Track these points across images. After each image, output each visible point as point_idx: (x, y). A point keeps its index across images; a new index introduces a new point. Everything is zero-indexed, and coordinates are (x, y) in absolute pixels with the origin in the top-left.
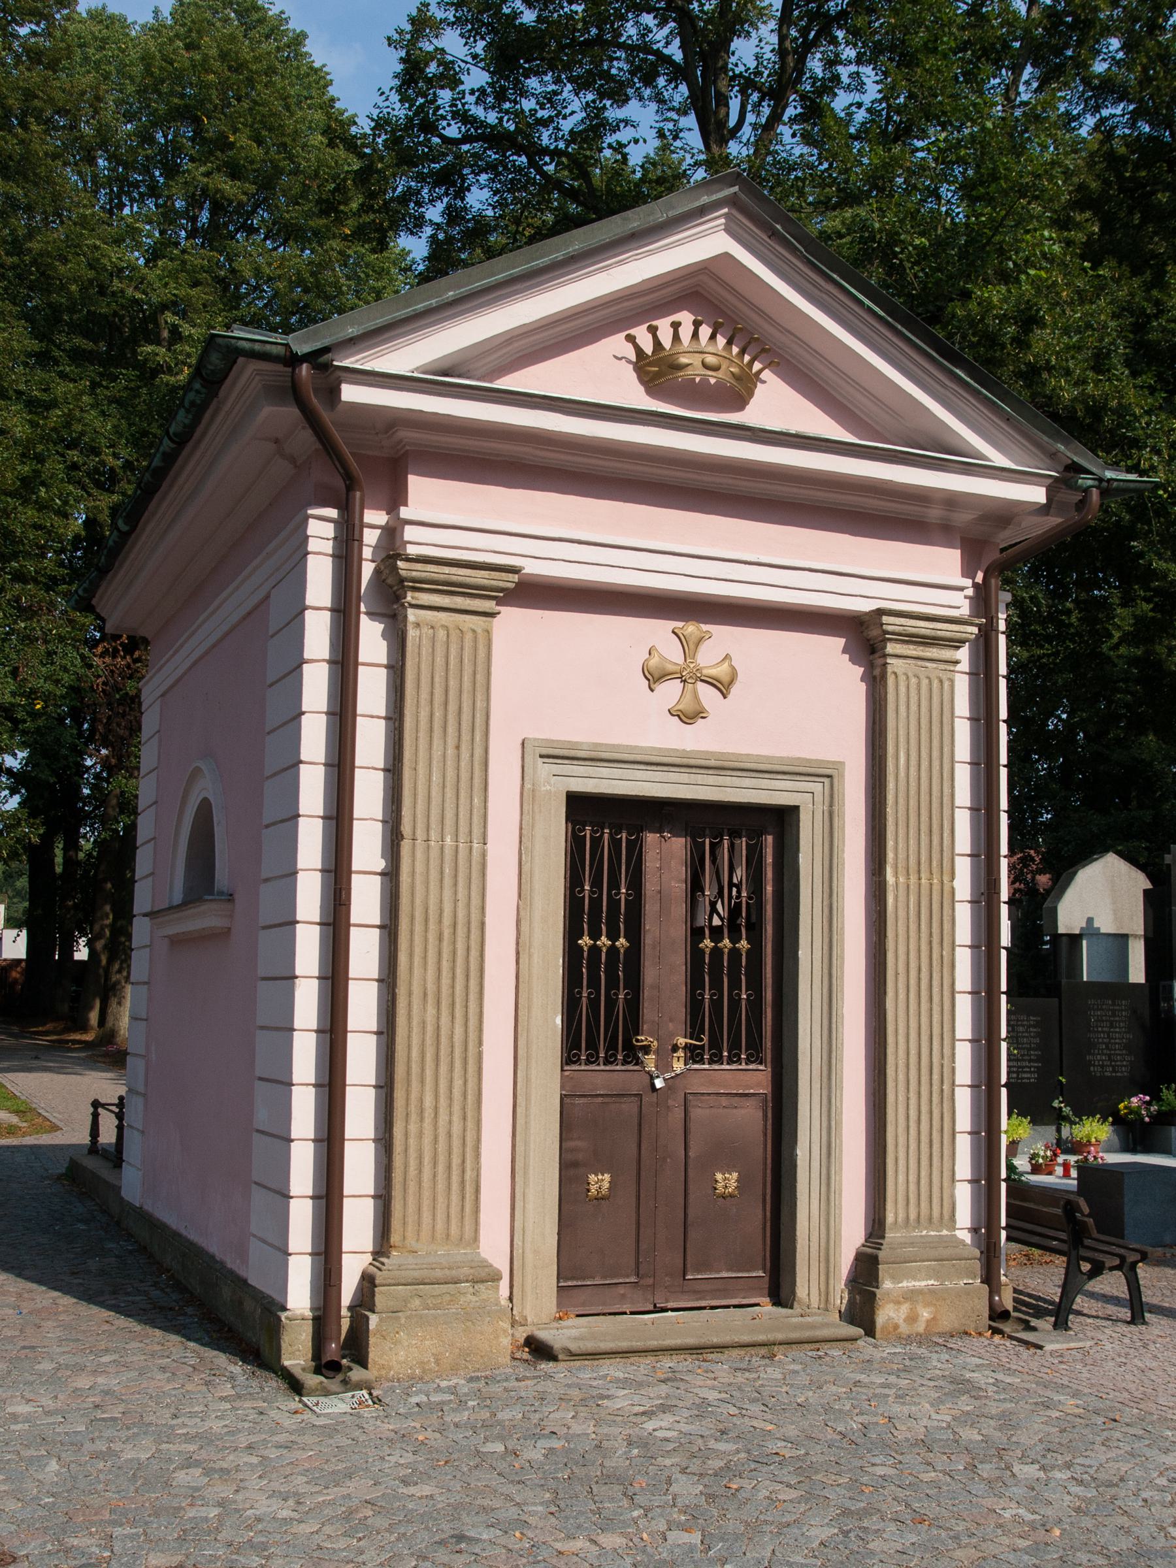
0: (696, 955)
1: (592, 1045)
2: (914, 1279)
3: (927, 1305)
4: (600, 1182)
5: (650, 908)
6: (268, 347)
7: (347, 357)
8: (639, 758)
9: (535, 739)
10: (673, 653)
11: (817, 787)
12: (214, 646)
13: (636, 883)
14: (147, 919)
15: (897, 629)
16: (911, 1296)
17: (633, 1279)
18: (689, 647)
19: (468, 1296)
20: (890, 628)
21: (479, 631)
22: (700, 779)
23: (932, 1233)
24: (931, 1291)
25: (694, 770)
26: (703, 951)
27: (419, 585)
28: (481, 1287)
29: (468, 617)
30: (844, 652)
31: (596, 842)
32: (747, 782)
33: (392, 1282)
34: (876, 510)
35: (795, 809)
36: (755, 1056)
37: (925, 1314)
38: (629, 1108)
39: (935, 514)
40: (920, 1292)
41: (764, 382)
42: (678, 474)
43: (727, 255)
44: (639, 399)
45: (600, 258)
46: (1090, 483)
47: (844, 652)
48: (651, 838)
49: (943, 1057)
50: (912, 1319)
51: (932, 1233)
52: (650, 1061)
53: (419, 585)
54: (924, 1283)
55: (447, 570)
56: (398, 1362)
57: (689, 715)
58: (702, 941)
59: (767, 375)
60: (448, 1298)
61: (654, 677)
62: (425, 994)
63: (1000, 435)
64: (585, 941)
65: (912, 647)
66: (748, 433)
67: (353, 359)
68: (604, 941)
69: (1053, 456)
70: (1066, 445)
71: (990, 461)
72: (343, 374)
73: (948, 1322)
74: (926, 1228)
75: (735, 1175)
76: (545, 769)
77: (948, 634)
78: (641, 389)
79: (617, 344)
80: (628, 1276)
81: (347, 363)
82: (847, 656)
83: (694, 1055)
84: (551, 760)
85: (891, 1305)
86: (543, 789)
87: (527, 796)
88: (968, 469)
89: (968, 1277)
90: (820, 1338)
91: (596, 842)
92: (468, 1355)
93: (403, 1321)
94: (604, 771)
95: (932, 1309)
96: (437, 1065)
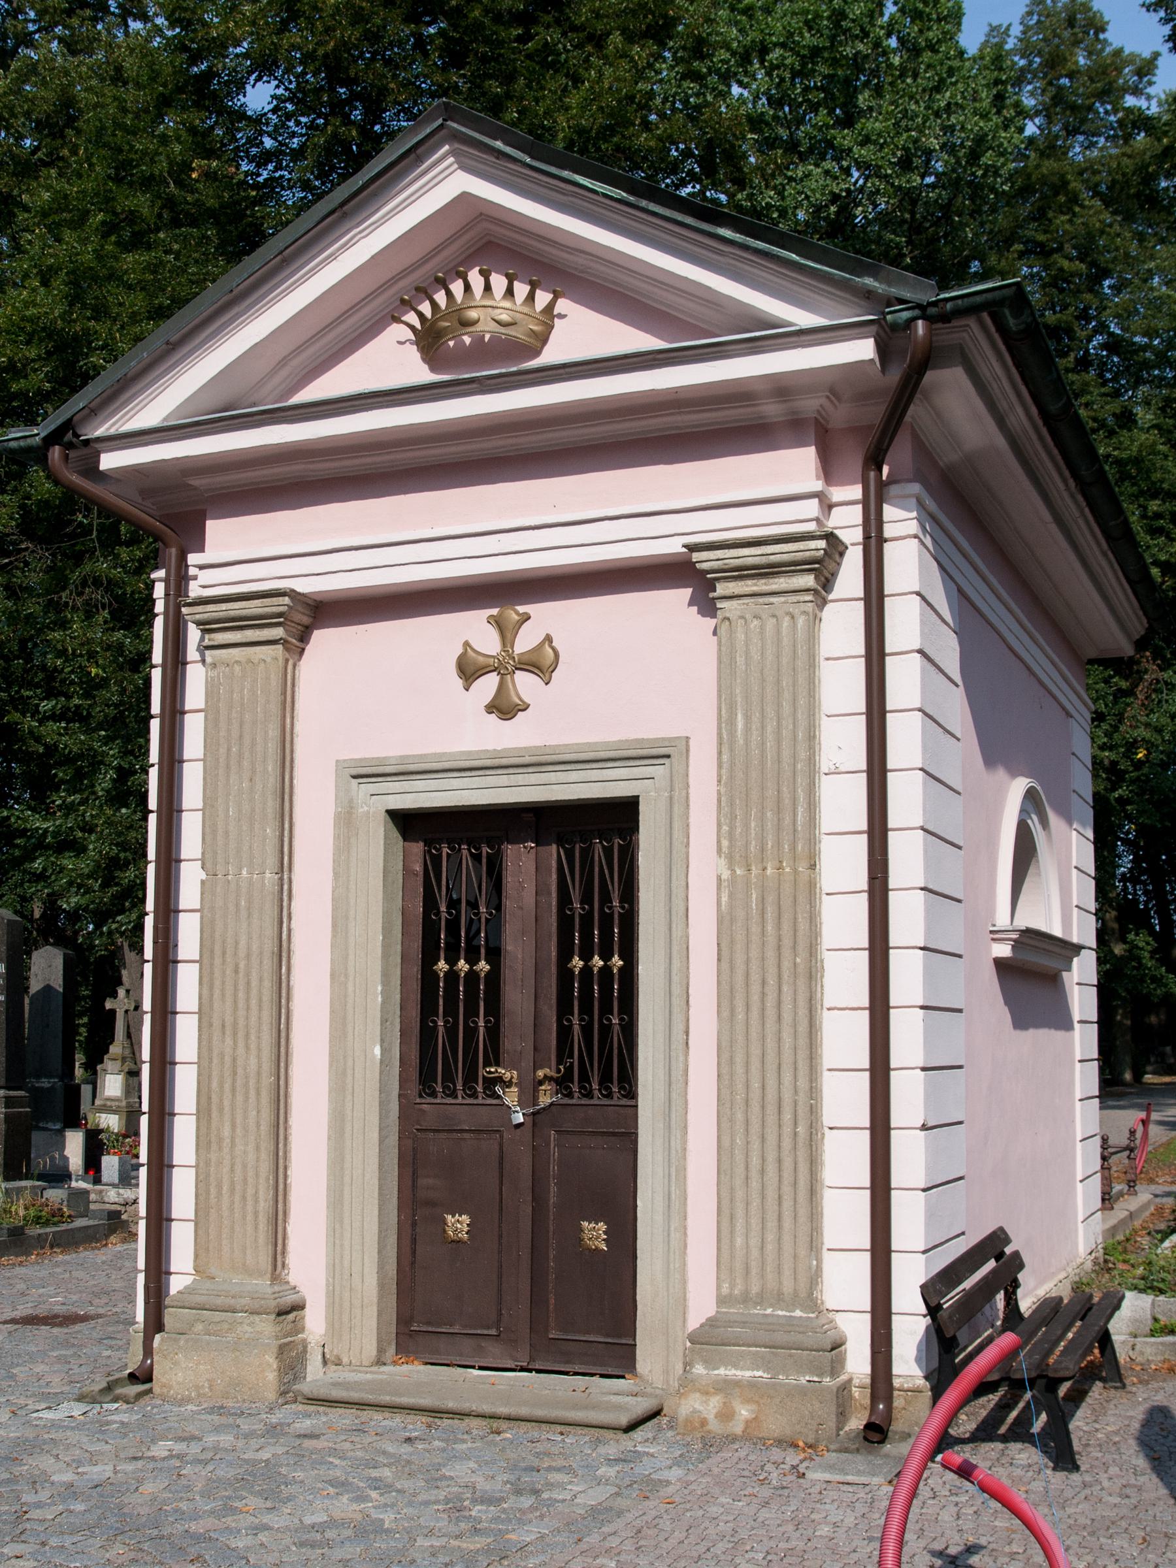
0: (565, 974)
1: (449, 1077)
2: (736, 1367)
3: (747, 1401)
4: (458, 1224)
6: (29, 441)
7: (96, 429)
8: (447, 765)
9: (345, 761)
10: (488, 643)
12: (1029, 668)
14: (922, 952)
15: (715, 565)
16: (726, 1387)
17: (493, 1332)
20: (705, 566)
21: (269, 660)
22: (520, 779)
23: (780, 1313)
24: (753, 1385)
25: (511, 771)
26: (571, 971)
28: (257, 1318)
29: (258, 649)
30: (690, 604)
32: (574, 776)
33: (179, 1304)
34: (694, 426)
37: (744, 1412)
39: (772, 410)
40: (737, 1383)
41: (561, 316)
42: (453, 449)
44: (422, 374)
45: (315, 251)
46: (906, 315)
47: (690, 604)
49: (796, 1092)
50: (726, 1415)
51: (780, 1313)
54: (748, 1374)
55: (224, 606)
56: (179, 1383)
58: (436, 964)
59: (563, 305)
60: (226, 1326)
61: (469, 671)
62: (223, 1026)
63: (795, 288)
65: (749, 582)
66: (474, 386)
67: (107, 426)
68: (463, 965)
69: (868, 295)
70: (875, 276)
71: (791, 324)
72: (98, 446)
73: (775, 1425)
74: (771, 1306)
75: (585, 1224)
76: (365, 789)
77: (786, 557)
78: (426, 367)
80: (488, 1328)
81: (100, 432)
82: (695, 608)
83: (562, 1083)
84: (365, 780)
85: (698, 1395)
86: (360, 810)
87: (346, 819)
88: (754, 346)
89: (812, 1373)
90: (570, 1420)
92: (238, 1385)
93: (182, 1343)
94: (420, 784)
95: (754, 1407)
96: (234, 1095)
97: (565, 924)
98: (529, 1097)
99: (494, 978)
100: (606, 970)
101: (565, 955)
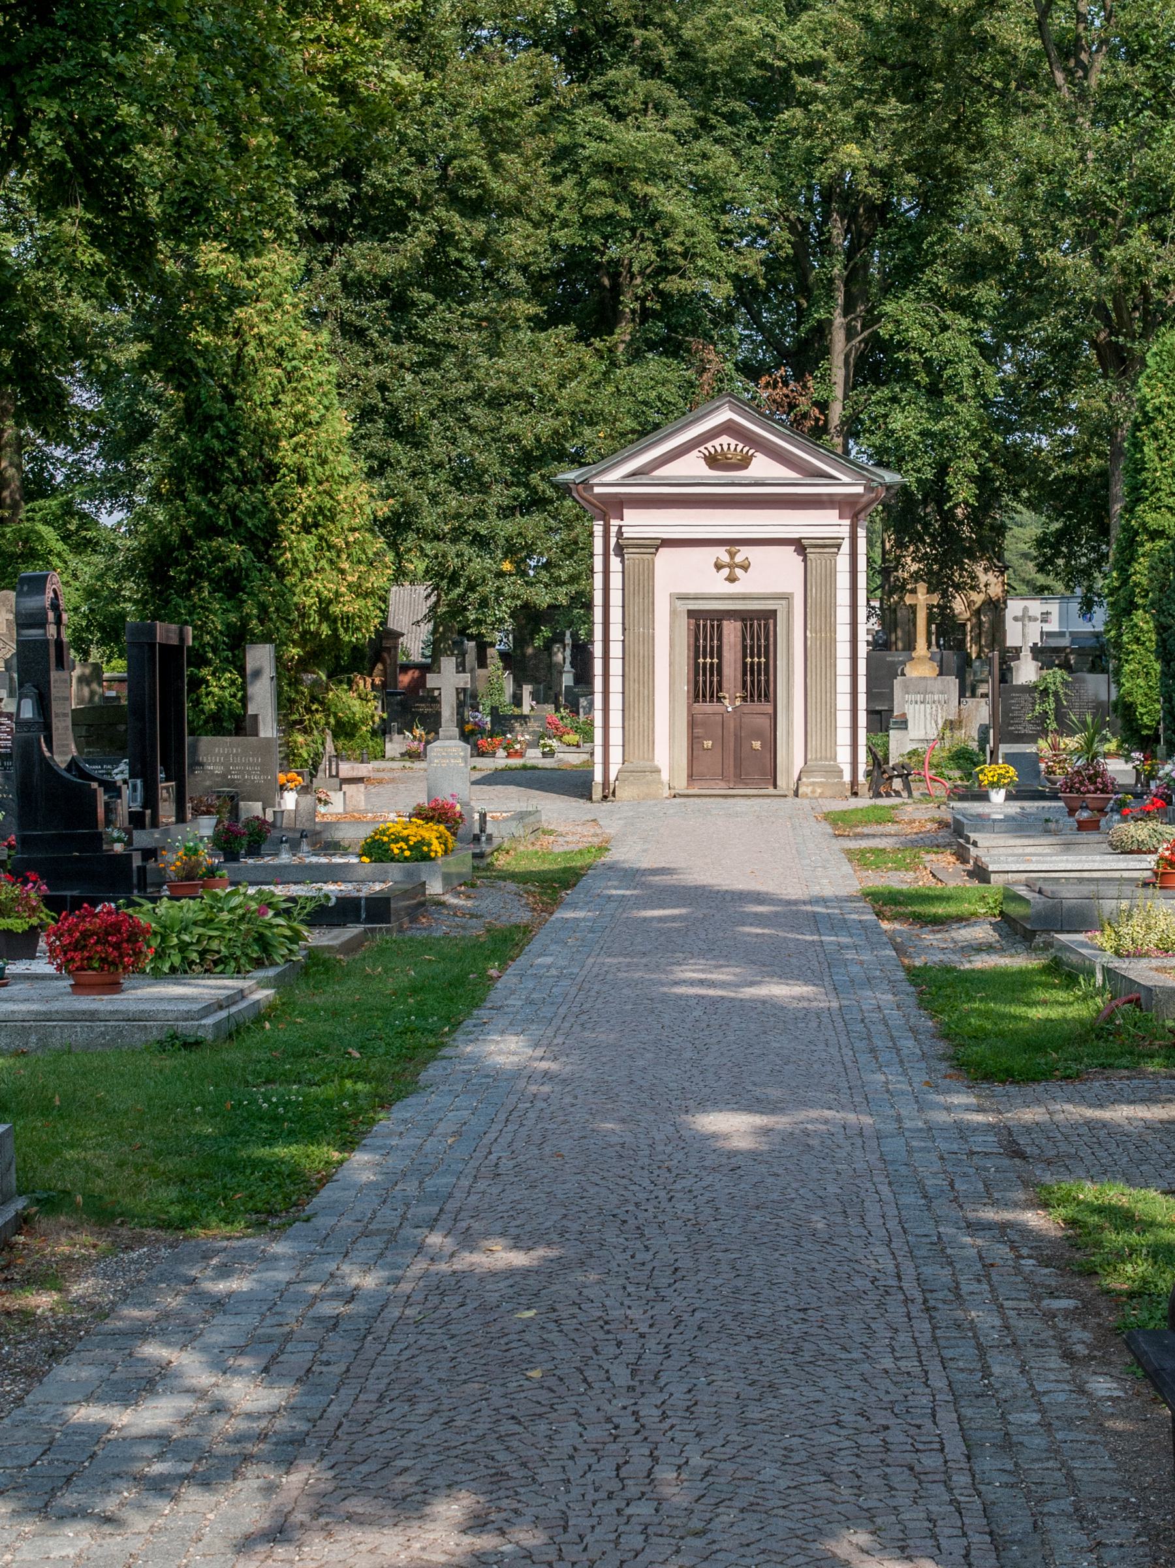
1: (704, 696)
4: (708, 744)
5: (725, 648)
10: (726, 558)
11: (784, 602)
13: (720, 639)
16: (813, 784)
18: (732, 555)
19: (649, 777)
27: (628, 546)
31: (705, 626)
35: (775, 611)
36: (767, 700)
37: (819, 791)
38: (719, 718)
43: (730, 420)
48: (725, 623)
50: (813, 792)
52: (726, 702)
53: (628, 546)
57: (732, 579)
61: (719, 567)
64: (701, 660)
76: (678, 603)
79: (695, 453)
83: (744, 699)
87: (673, 613)
91: (705, 626)
97: (744, 647)
98: (732, 702)
99: (720, 665)
100: (759, 663)
101: (744, 657)
